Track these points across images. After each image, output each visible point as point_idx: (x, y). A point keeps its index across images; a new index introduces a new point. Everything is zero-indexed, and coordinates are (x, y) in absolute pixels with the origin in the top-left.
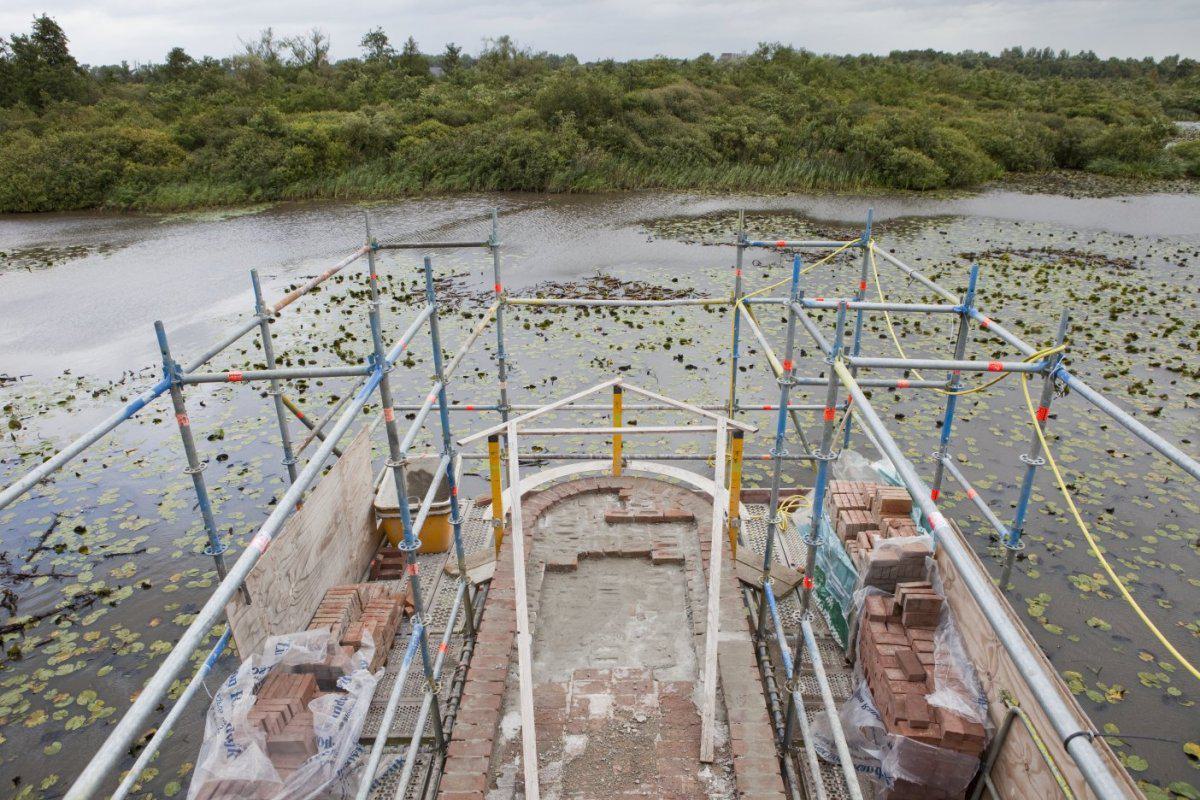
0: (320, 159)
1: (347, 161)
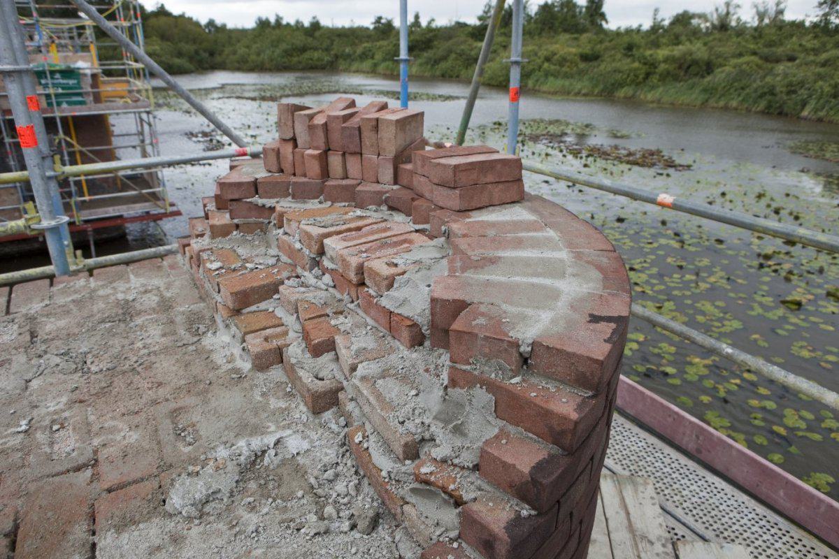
0: (648, 75)
1: (666, 77)
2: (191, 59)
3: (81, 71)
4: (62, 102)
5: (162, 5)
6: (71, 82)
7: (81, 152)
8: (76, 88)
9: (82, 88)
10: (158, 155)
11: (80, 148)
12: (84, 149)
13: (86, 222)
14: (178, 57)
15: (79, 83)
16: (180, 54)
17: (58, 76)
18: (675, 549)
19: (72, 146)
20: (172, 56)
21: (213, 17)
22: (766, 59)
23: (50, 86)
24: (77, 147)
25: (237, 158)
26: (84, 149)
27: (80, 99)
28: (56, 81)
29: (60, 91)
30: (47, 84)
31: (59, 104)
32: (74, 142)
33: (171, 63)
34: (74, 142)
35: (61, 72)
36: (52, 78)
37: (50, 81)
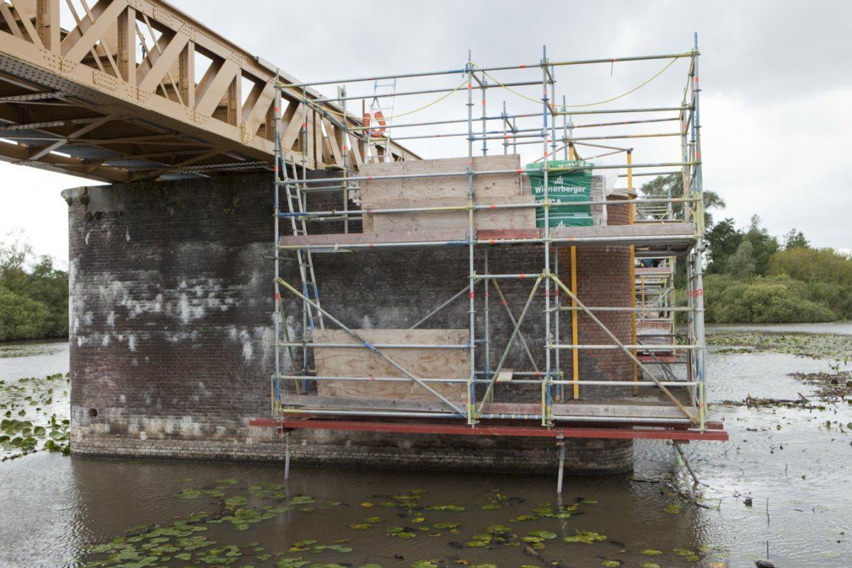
2: (832, 304)
3: (595, 173)
4: (559, 221)
5: (801, 234)
6: (576, 190)
7: (581, 314)
8: (582, 199)
9: (591, 199)
10: (689, 344)
11: (583, 307)
12: (587, 309)
13: (559, 424)
14: (813, 300)
15: (588, 192)
16: (816, 297)
17: (560, 180)
18: (473, 88)
19: (568, 301)
20: (803, 298)
21: (802, 359)
22: (697, 374)
23: (546, 195)
24: (577, 305)
25: (43, 131)
26: (587, 309)
27: (585, 216)
28: (555, 189)
29: (559, 203)
30: (542, 193)
31: (553, 224)
32: (573, 295)
33: (799, 306)
34: (573, 295)
35: (565, 174)
36: (550, 184)
37: (546, 189)
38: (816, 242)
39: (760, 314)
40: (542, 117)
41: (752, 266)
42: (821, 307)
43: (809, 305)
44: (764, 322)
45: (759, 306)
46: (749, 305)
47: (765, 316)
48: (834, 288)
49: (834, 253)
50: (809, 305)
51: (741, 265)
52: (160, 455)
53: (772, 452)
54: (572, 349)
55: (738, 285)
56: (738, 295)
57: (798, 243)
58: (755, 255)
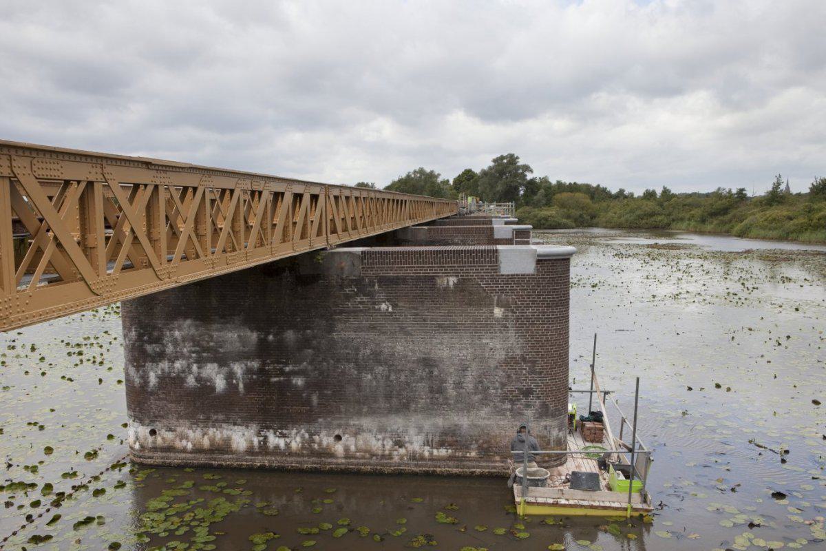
2: (576, 220)
16: (569, 217)
38: (675, 190)
39: (544, 224)
40: (589, 393)
41: (544, 202)
42: (569, 222)
43: (564, 221)
44: (545, 228)
45: (543, 221)
46: (539, 221)
47: (546, 226)
48: (577, 213)
49: (440, 179)
50: (564, 221)
51: (539, 201)
52: (156, 463)
53: (783, 461)
54: (599, 489)
55: (536, 211)
56: (535, 216)
57: (666, 192)
58: (546, 196)
